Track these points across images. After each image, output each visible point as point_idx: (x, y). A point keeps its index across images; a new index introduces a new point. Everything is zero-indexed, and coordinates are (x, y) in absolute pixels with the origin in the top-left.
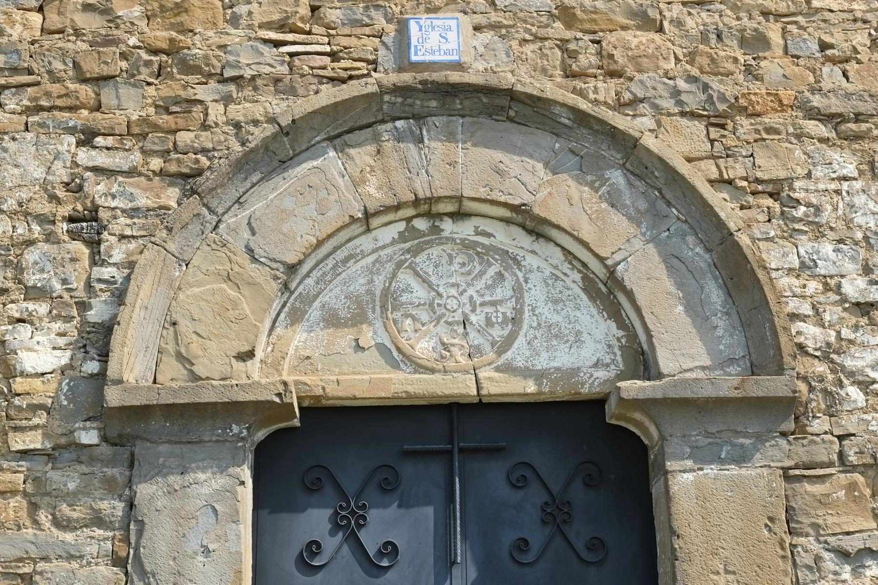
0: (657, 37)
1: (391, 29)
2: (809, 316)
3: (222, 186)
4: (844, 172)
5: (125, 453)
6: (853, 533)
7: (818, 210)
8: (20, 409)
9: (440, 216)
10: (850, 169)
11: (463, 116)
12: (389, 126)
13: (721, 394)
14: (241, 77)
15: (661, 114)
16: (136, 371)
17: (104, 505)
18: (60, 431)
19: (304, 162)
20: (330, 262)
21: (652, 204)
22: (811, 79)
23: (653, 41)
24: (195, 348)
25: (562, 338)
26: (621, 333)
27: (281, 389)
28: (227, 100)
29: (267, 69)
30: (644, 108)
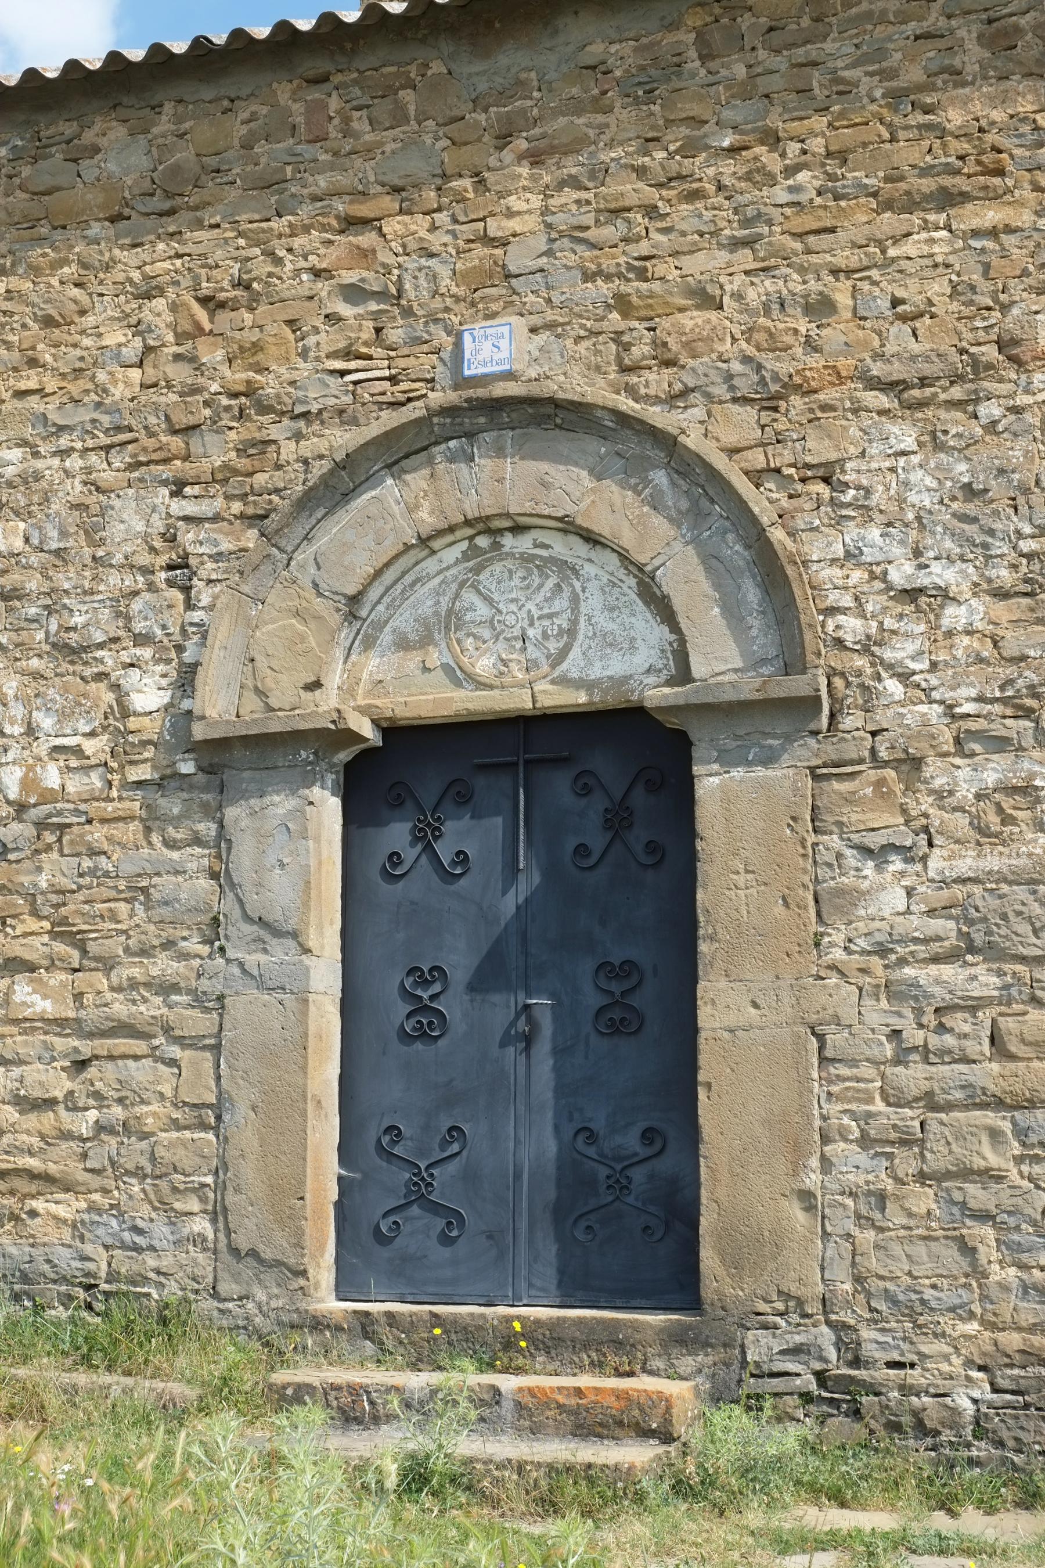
0: (713, 315)
1: (448, 341)
2: (850, 608)
3: (288, 526)
4: (902, 446)
5: (215, 779)
6: (878, 829)
7: (868, 492)
8: (133, 745)
9: (500, 531)
10: (909, 443)
11: (513, 429)
12: (443, 446)
13: (742, 697)
14: (309, 412)
15: (713, 403)
16: (219, 707)
17: (201, 827)
18: (165, 763)
19: (365, 492)
20: (399, 587)
21: (695, 503)
22: (876, 343)
23: (709, 321)
24: (270, 683)
25: (616, 646)
26: (673, 637)
27: (335, 716)
28: (298, 436)
29: (332, 401)
30: (695, 398)
